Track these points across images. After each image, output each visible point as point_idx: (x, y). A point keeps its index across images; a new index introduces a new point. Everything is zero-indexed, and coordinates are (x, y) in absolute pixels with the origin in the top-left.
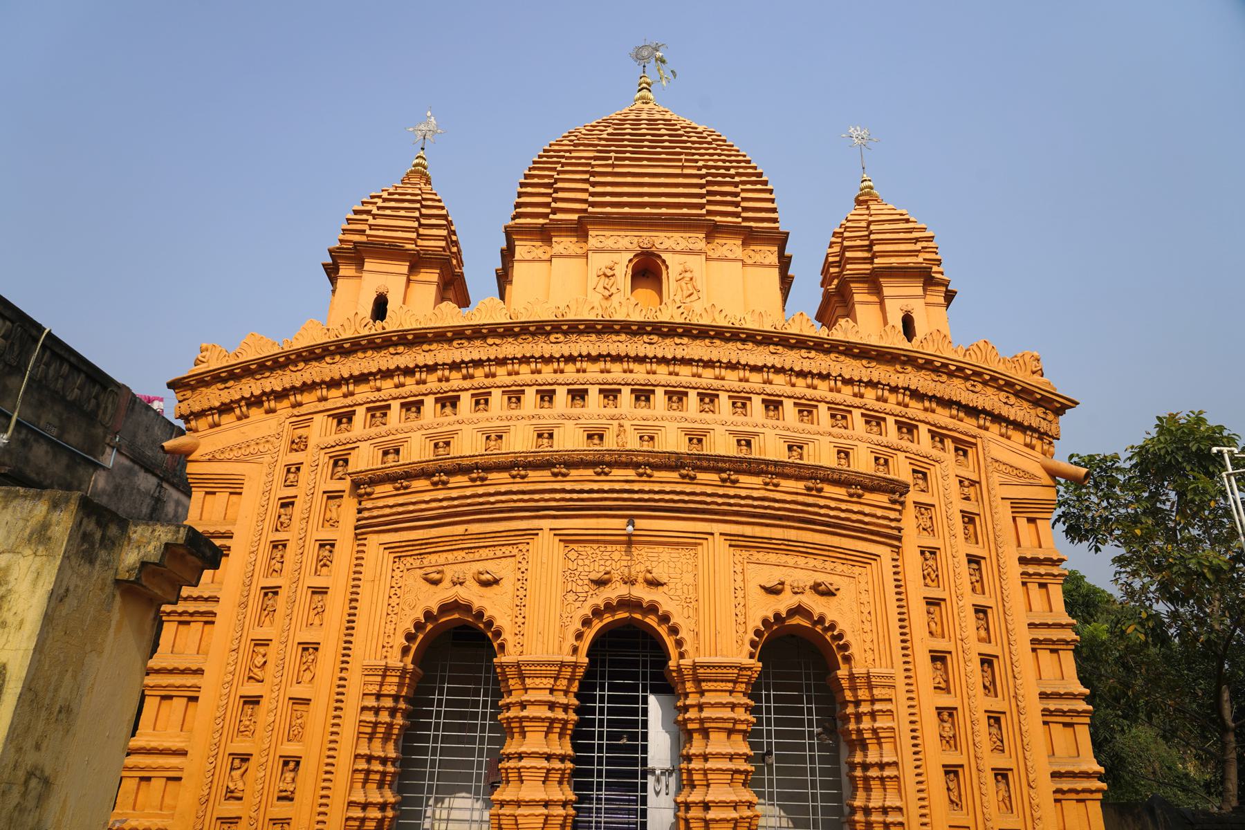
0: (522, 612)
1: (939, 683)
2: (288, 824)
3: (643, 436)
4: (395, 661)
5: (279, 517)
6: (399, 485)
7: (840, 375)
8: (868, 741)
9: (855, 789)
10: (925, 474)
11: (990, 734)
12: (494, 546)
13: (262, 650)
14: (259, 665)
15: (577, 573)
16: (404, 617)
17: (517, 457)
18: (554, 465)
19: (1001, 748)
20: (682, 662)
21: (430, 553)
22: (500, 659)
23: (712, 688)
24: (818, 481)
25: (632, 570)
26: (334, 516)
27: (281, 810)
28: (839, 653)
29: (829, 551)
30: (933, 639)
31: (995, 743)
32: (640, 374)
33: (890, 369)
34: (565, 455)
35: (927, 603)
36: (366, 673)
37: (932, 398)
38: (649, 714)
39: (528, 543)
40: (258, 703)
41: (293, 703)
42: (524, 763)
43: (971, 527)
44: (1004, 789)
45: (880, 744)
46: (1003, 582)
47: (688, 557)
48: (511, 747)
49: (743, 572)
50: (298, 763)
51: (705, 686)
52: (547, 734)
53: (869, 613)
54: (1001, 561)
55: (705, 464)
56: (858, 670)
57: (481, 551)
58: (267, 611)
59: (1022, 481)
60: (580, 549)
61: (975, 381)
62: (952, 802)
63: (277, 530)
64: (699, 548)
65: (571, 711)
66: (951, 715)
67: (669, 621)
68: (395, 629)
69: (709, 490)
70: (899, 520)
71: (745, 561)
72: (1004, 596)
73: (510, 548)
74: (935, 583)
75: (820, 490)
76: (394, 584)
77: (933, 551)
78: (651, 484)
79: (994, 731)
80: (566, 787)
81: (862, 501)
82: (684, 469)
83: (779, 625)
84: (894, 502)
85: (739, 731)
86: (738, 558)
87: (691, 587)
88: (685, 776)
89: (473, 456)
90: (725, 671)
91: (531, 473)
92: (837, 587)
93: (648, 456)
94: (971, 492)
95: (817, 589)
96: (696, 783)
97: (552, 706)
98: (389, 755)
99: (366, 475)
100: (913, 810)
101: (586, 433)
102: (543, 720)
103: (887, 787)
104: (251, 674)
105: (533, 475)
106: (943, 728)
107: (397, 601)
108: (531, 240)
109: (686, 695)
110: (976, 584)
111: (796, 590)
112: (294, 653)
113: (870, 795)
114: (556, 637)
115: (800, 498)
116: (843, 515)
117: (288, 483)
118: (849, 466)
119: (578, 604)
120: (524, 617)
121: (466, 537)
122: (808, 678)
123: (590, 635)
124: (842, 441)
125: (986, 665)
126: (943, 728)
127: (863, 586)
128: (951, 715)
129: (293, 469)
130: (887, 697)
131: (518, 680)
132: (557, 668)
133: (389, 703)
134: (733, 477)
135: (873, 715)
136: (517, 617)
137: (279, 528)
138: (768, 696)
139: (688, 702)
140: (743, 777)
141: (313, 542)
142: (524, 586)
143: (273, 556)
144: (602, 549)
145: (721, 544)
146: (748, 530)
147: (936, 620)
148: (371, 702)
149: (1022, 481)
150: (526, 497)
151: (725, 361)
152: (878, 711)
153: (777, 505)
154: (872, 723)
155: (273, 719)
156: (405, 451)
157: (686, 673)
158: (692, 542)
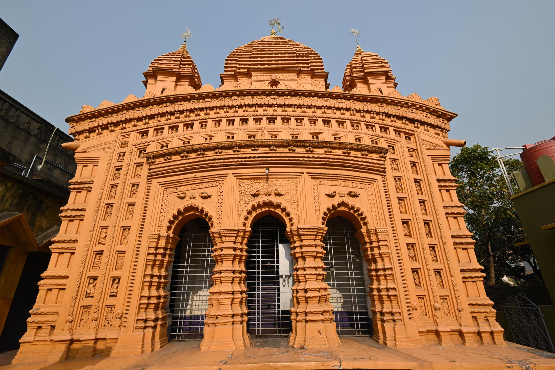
2: (114, 307)
4: (164, 232)
6: (166, 158)
7: (355, 109)
10: (393, 147)
13: (105, 231)
15: (245, 192)
16: (168, 213)
17: (218, 144)
20: (292, 227)
23: (306, 238)
27: (111, 301)
32: (270, 111)
33: (376, 105)
35: (399, 200)
36: (150, 238)
37: (394, 116)
38: (279, 252)
39: (223, 180)
40: (102, 254)
45: (383, 260)
50: (119, 280)
51: (302, 237)
52: (233, 262)
53: (374, 204)
55: (299, 144)
56: (371, 227)
57: (203, 184)
59: (435, 148)
60: (246, 182)
61: (412, 108)
62: (416, 284)
64: (298, 179)
65: (244, 251)
66: (413, 247)
69: (301, 155)
70: (384, 165)
71: (318, 184)
74: (401, 191)
75: (349, 153)
76: (164, 200)
79: (433, 253)
80: (242, 285)
81: (368, 157)
85: (319, 257)
86: (315, 183)
88: (295, 278)
89: (198, 144)
90: (311, 230)
91: (224, 151)
93: (274, 142)
95: (350, 194)
96: (301, 280)
97: (235, 249)
98: (162, 274)
99: (151, 154)
101: (248, 135)
102: (231, 255)
104: (100, 241)
105: (225, 152)
108: (230, 80)
109: (295, 242)
111: (341, 195)
112: (119, 231)
115: (341, 157)
117: (119, 160)
119: (245, 205)
122: (347, 234)
123: (251, 218)
124: (357, 134)
127: (370, 193)
128: (413, 247)
129: (122, 155)
130: (385, 239)
134: (311, 149)
135: (379, 247)
139: (295, 245)
140: (322, 277)
141: (129, 183)
145: (307, 177)
146: (319, 171)
148: (153, 251)
149: (435, 148)
151: (306, 104)
152: (381, 245)
153: (331, 160)
157: (294, 232)
158: (294, 177)
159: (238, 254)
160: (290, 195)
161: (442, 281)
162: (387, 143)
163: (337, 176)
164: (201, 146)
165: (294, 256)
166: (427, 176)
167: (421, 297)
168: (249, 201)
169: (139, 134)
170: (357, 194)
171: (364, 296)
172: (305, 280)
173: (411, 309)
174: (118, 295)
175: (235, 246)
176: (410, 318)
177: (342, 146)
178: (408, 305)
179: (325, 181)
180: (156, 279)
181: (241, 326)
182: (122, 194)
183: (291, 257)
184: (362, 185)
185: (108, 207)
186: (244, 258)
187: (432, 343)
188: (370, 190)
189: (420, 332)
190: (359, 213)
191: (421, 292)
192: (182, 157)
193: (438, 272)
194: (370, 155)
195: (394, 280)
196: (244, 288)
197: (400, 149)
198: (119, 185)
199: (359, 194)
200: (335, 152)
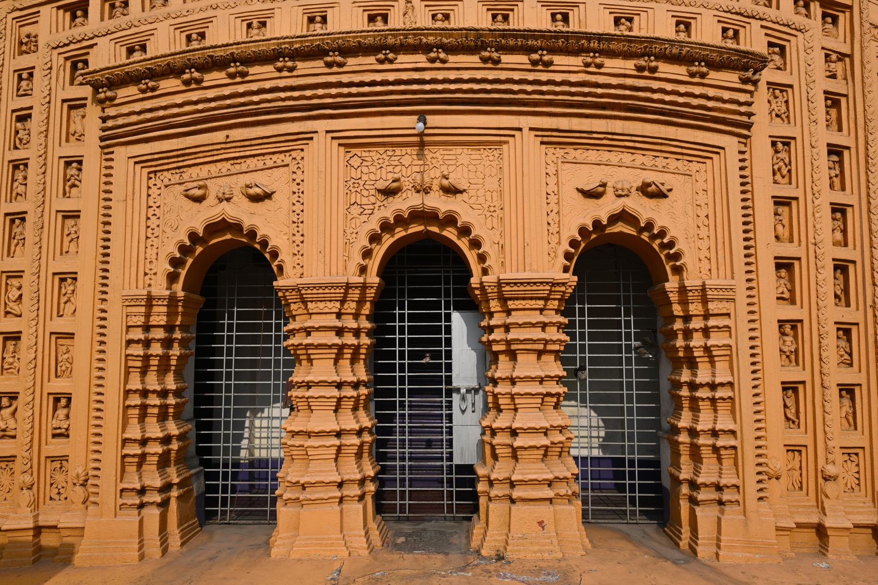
0: (300, 229)
1: (783, 293)
2: (67, 460)
3: (436, 15)
4: (160, 289)
5: (17, 132)
6: (144, 87)
8: (698, 360)
9: (679, 408)
10: (782, 48)
11: (838, 347)
12: (263, 155)
13: (15, 282)
14: (14, 299)
15: (362, 183)
16: (165, 240)
17: (281, 44)
18: (326, 53)
19: (848, 362)
20: (485, 279)
21: (189, 166)
22: (279, 283)
23: (521, 307)
24: (652, 58)
25: (426, 176)
26: (79, 129)
27: (56, 447)
28: (668, 264)
29: (661, 144)
30: (779, 244)
31: (842, 356)
34: (339, 38)
35: (776, 203)
36: (127, 303)
38: (453, 332)
39: (302, 150)
40: (19, 338)
41: (57, 338)
42: (312, 392)
43: (833, 112)
44: (848, 405)
45: (712, 363)
46: (871, 176)
47: (491, 158)
48: (299, 375)
49: (557, 174)
50: (69, 399)
51: (511, 304)
52: (336, 361)
53: (707, 216)
54: (871, 150)
55: (511, 42)
56: (692, 281)
57: (249, 161)
58: (14, 240)
60: (364, 154)
62: (788, 419)
63: (16, 148)
64: (505, 147)
65: (363, 335)
66: (794, 328)
67: (470, 234)
68: (157, 254)
69: (516, 76)
70: (749, 104)
71: (560, 161)
72: (871, 192)
73: (282, 156)
74: (786, 179)
75: (654, 70)
76: (151, 204)
77: (787, 142)
78: (446, 72)
79: (843, 343)
80: (361, 413)
81: (705, 81)
82: (486, 50)
83: (598, 234)
84: (745, 81)
85: (551, 352)
86: (551, 158)
87: (495, 194)
88: (490, 399)
89: (227, 45)
90: (535, 288)
91: (300, 65)
92: (670, 187)
93: (441, 35)
94: (838, 68)
95: (645, 190)
96: (502, 407)
97: (340, 332)
98: (169, 387)
99: (102, 76)
100: (749, 433)
101: (366, 13)
102: (330, 347)
103: (718, 408)
104: (8, 309)
105: (303, 67)
106: (784, 341)
107: (157, 222)
109: (491, 315)
110: (835, 179)
111: (620, 192)
112: (49, 286)
113: (698, 417)
114: (340, 256)
115: (629, 82)
116: (681, 100)
117: (21, 92)
118: (689, 36)
119: (364, 218)
120: (302, 235)
121: (228, 145)
122: (626, 289)
123: (380, 252)
124: (683, 8)
125: (839, 271)
126: (784, 341)
127: (701, 185)
128: (794, 328)
129: (25, 76)
130: (725, 311)
131: (301, 305)
132: (342, 291)
133: (160, 334)
134: (546, 58)
135: (706, 332)
136: (294, 235)
137: (18, 146)
138: (582, 311)
139: (492, 323)
140: (555, 400)
141: (56, 159)
142: (300, 199)
143: (15, 179)
144: (389, 153)
145: (531, 141)
146: (564, 123)
147: (784, 222)
148: (138, 334)
150: (296, 94)
152: (713, 327)
153: (599, 91)
154: (705, 339)
155: (33, 356)
156: (153, 47)
157: (489, 290)
159: (349, 342)
160: (481, 192)
161: (854, 413)
162: (766, 34)
163: (615, 137)
164: (233, 49)
165: (488, 348)
166: (866, 137)
167: (793, 449)
168: (371, 207)
169: (61, 12)
170: (664, 189)
171: (655, 438)
172: (512, 407)
173: (766, 476)
174: (71, 433)
175: (339, 324)
176: (760, 499)
177: (637, 48)
178: (760, 469)
179: (580, 151)
180: (154, 400)
181: (360, 506)
182: (42, 187)
183: (480, 346)
184: (679, 164)
185: (12, 221)
186: (363, 351)
187: (805, 550)
188: (701, 177)
189: (778, 529)
190: (665, 241)
191: (797, 437)
192: (186, 83)
193: (848, 391)
194: (713, 74)
195: (733, 412)
196: (367, 422)
197: (802, 54)
198: (31, 163)
199: (670, 190)
200: (613, 65)
